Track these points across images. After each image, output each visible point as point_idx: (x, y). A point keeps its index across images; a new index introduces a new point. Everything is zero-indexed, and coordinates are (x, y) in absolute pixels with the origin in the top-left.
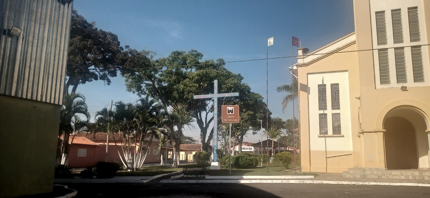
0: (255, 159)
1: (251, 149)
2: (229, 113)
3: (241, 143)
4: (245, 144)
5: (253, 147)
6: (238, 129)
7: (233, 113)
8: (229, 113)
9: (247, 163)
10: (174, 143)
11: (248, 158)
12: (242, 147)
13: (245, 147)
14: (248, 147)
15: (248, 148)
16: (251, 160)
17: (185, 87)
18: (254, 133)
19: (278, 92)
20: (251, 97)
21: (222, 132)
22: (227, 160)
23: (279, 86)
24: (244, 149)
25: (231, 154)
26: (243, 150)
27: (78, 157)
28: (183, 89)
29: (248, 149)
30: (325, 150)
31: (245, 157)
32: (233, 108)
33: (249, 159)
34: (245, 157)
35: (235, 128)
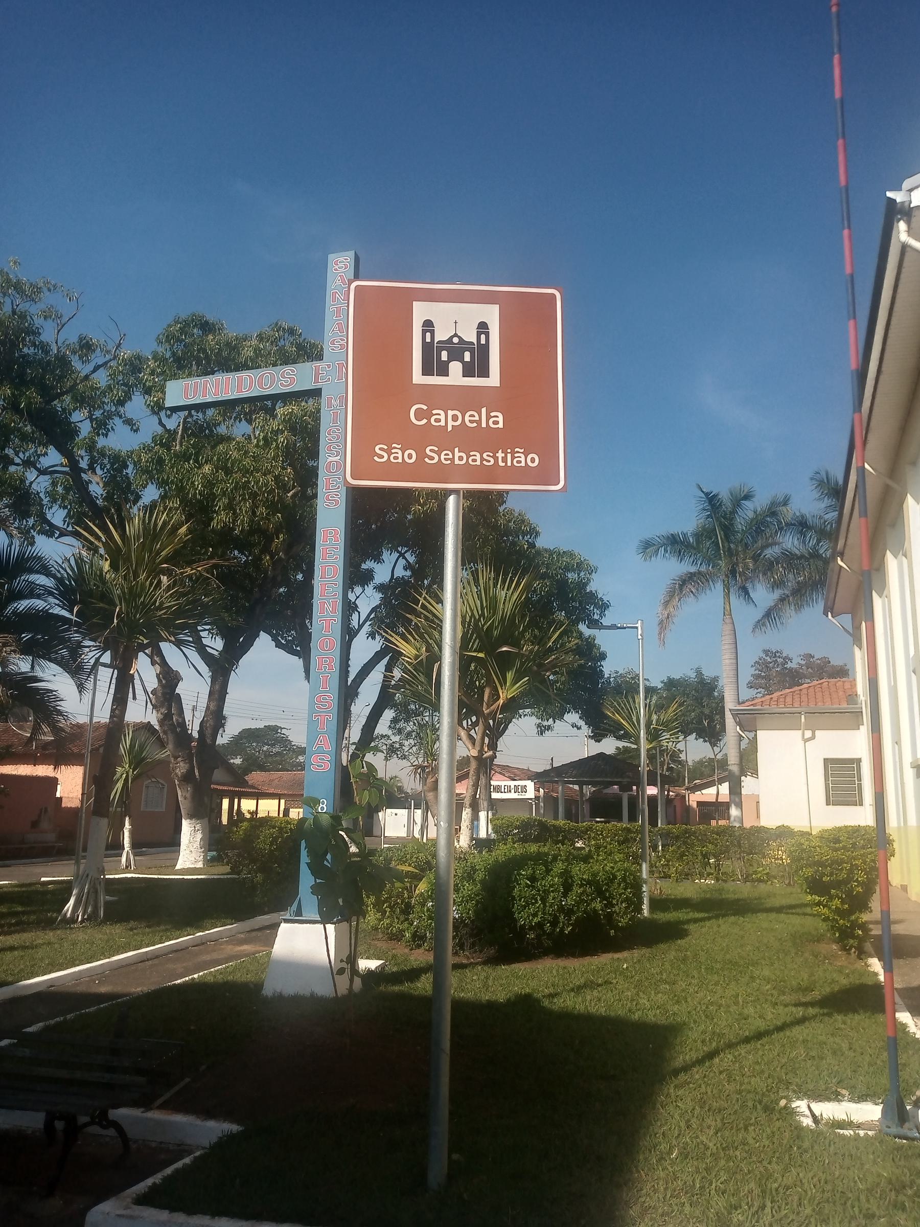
0: (624, 879)
1: (524, 789)
2: (443, 371)
3: (491, 769)
4: (500, 773)
5: (530, 785)
6: (505, 662)
7: (494, 379)
8: (443, 371)
9: (569, 912)
10: (182, 764)
11: (579, 871)
12: (493, 783)
13: (502, 783)
14: (512, 784)
15: (512, 787)
16: (600, 888)
17: (221, 474)
18: (542, 730)
19: (645, 560)
20: (543, 563)
21: (414, 724)
22: (422, 887)
23: (648, 535)
24: (498, 789)
25: (456, 844)
26: (494, 795)
27: (66, 808)
28: (209, 484)
29: (513, 791)
30: (716, 793)
31: (559, 867)
32: (492, 314)
33: (589, 883)
34: (559, 867)
35: (481, 655)
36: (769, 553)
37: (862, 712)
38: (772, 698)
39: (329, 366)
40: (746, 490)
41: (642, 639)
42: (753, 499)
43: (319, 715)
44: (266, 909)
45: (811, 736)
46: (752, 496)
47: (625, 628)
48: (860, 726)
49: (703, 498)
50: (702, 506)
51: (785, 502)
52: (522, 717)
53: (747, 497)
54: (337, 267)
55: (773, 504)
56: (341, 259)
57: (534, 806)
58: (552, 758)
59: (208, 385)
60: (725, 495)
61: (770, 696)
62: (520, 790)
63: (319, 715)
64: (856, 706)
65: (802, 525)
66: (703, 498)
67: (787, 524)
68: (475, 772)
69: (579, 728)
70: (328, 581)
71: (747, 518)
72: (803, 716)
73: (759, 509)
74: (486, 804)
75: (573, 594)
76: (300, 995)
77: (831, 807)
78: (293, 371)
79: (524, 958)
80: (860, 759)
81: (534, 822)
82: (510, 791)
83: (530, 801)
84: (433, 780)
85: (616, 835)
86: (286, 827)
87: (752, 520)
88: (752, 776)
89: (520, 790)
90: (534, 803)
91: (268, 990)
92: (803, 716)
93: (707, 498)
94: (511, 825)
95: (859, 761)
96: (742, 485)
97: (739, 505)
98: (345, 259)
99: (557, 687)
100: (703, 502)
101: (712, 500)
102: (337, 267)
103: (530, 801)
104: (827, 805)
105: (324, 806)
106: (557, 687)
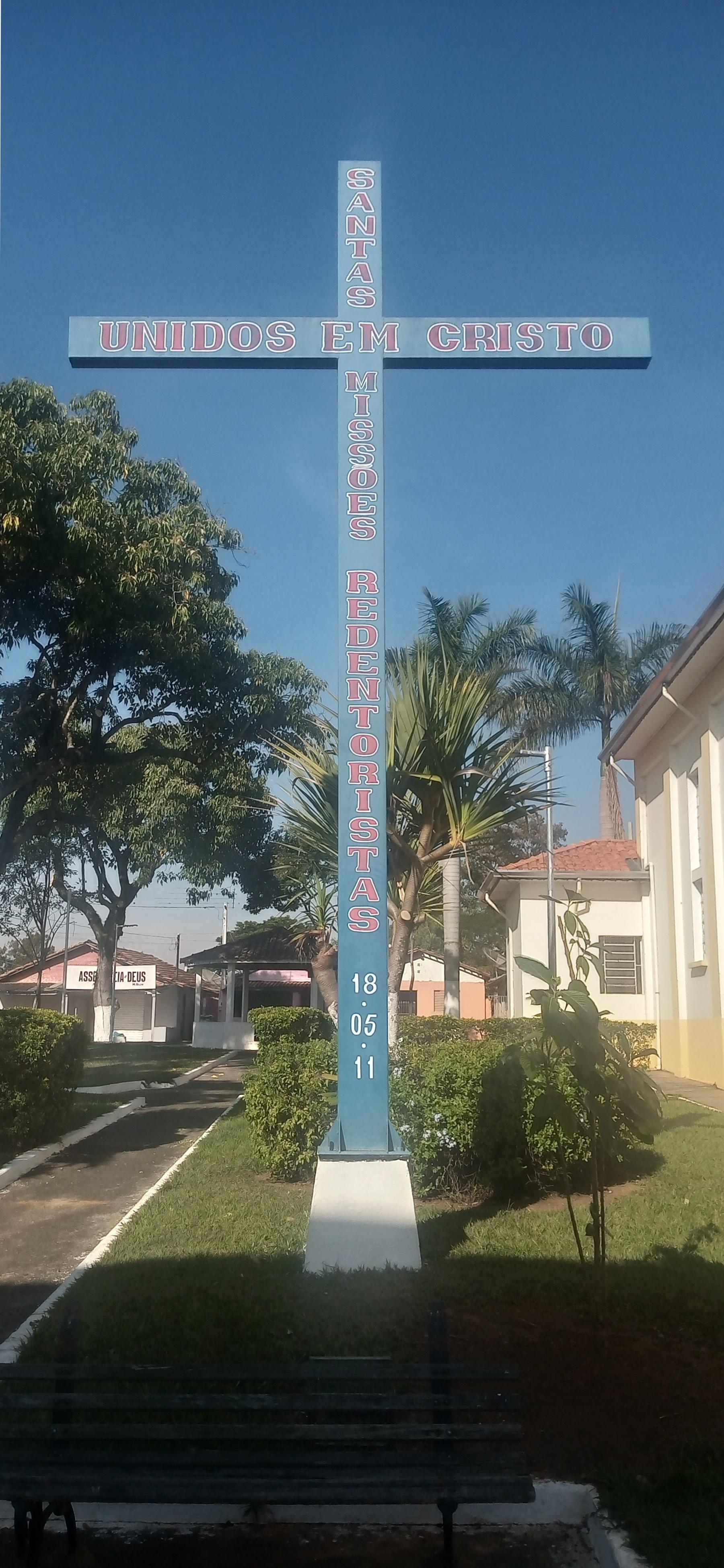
1: (142, 976)
15: (126, 974)
18: (194, 898)
29: (126, 979)
36: (505, 683)
37: (649, 880)
38: (538, 860)
39: (348, 327)
40: (479, 602)
41: (550, 771)
42: (486, 614)
43: (357, 850)
44: (19, 1145)
45: (585, 908)
46: (486, 611)
47: (529, 755)
48: (643, 897)
49: (429, 606)
50: (426, 618)
51: (529, 621)
52: (168, 880)
53: (479, 611)
54: (353, 181)
55: (512, 621)
56: (360, 171)
57: (154, 999)
58: (179, 936)
59: (144, 331)
60: (454, 608)
61: (536, 857)
62: (135, 979)
63: (357, 850)
64: (640, 872)
65: (542, 650)
66: (429, 606)
67: (528, 647)
68: (403, 943)
69: (231, 896)
70: (363, 650)
71: (481, 636)
72: (579, 883)
73: (495, 627)
74: (105, 996)
75: (291, 717)
76: (369, 1270)
77: (605, 995)
78: (289, 327)
79: (527, 1198)
80: (641, 937)
81: (314, 1016)
82: (122, 980)
83: (149, 993)
84: (328, 953)
85: (415, 1030)
86: (59, 1024)
87: (486, 640)
88: (437, 961)
89: (135, 979)
90: (154, 995)
91: (314, 1265)
92: (579, 883)
93: (433, 606)
94: (286, 1020)
95: (639, 939)
96: (475, 596)
97: (470, 619)
98: (367, 172)
99: (218, 842)
100: (429, 612)
101: (439, 608)
102: (353, 181)
103: (149, 993)
104: (601, 993)
105: (372, 983)
106: (218, 842)
